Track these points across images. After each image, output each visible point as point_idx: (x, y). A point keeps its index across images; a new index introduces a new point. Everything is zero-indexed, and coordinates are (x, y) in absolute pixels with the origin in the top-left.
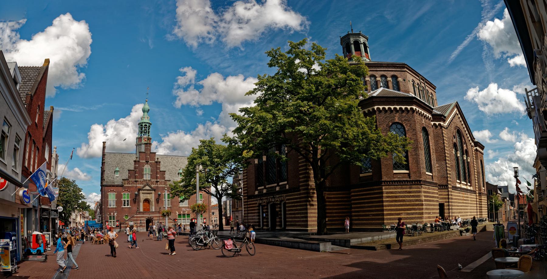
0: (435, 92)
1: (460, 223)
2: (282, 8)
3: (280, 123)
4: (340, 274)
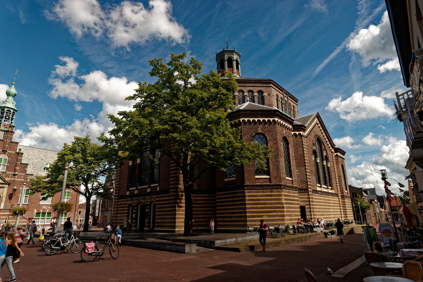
0: (297, 105)
1: (323, 225)
2: (167, 18)
3: (156, 129)
4: (203, 277)
